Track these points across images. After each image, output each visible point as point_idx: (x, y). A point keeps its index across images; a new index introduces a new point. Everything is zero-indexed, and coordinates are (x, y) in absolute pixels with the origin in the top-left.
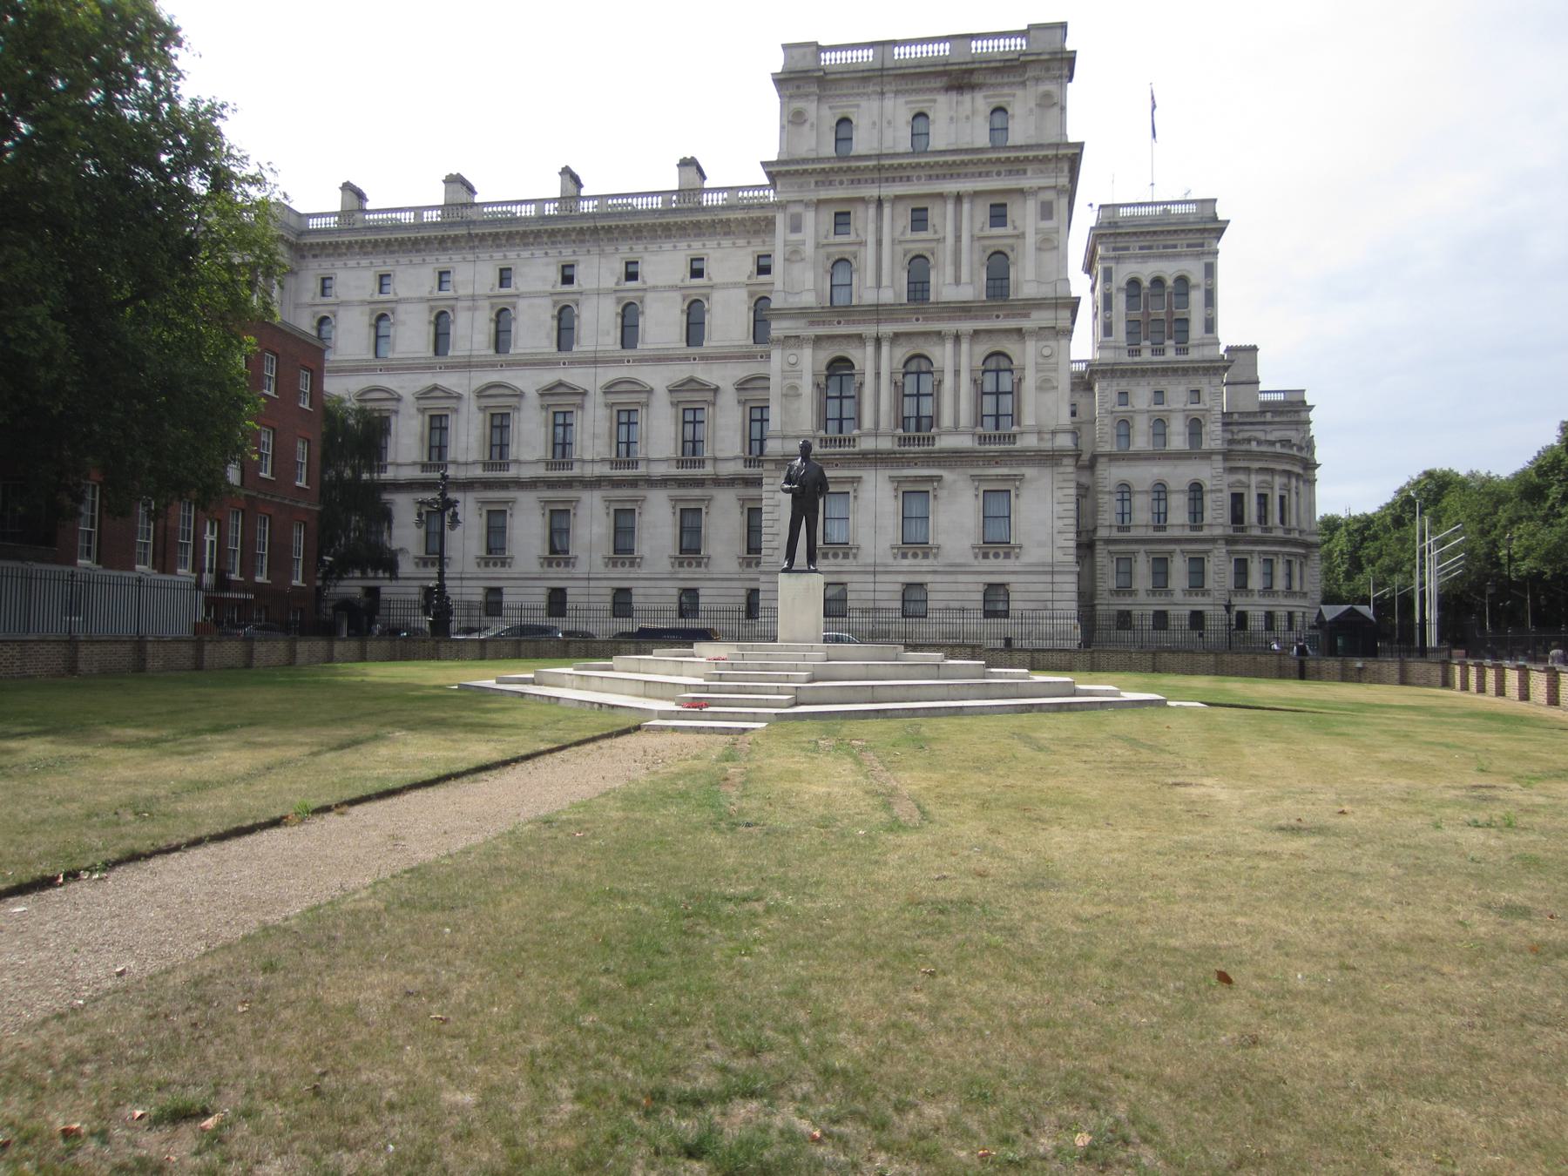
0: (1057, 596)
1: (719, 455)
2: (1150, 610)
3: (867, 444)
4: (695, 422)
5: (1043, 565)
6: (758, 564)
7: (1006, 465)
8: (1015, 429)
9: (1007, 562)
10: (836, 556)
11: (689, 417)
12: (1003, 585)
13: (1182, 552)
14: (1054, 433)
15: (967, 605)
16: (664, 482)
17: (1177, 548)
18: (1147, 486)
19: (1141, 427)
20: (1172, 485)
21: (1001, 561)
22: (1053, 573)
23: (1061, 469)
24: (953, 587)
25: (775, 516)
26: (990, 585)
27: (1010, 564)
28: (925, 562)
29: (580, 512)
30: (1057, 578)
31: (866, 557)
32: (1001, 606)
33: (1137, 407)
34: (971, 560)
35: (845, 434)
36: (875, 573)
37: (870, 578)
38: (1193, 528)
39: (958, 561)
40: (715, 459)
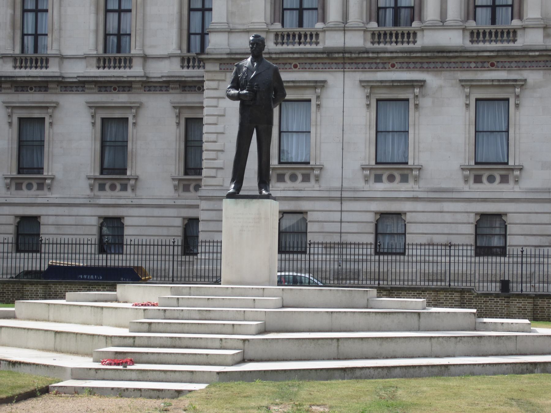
1: (150, 52)
6: (197, 187)
7: (503, 68)
8: (516, 23)
9: (504, 186)
10: (293, 178)
12: (499, 215)
15: (455, 240)
16: (81, 85)
24: (438, 217)
25: (219, 128)
28: (404, 186)
29: (141, 121)
31: (331, 178)
32: (496, 242)
34: (461, 185)
35: (306, 28)
37: (336, 205)
39: (444, 185)
40: (145, 58)
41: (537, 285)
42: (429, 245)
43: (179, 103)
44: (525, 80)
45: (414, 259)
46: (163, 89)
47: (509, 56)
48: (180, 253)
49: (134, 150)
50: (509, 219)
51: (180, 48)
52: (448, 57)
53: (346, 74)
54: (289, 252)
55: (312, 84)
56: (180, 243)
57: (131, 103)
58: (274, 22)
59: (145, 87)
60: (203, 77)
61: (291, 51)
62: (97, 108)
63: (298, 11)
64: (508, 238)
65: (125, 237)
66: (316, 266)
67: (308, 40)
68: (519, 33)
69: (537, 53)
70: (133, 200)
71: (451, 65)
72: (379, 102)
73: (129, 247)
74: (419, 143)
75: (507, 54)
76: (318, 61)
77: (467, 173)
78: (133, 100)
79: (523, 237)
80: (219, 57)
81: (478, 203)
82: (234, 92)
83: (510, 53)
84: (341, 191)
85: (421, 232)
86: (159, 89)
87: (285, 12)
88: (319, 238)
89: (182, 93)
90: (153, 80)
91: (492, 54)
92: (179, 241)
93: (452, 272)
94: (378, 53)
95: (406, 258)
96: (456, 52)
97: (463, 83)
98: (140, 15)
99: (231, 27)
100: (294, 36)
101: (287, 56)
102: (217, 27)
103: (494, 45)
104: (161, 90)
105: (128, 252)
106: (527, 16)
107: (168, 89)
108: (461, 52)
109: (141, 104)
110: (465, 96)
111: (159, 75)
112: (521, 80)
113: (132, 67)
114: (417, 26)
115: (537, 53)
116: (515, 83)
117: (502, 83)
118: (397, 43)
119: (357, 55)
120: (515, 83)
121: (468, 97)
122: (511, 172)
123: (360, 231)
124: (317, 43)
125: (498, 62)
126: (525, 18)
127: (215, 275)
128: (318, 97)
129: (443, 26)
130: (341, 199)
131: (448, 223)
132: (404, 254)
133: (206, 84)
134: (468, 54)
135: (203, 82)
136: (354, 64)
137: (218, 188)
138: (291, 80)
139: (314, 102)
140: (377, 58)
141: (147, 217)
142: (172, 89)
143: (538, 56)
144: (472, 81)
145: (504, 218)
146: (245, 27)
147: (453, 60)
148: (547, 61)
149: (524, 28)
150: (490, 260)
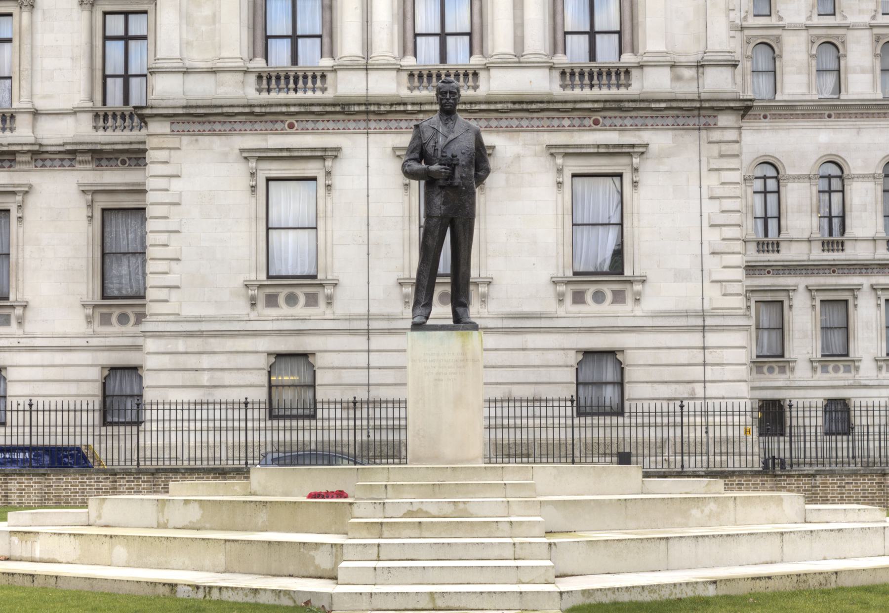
0: (711, 373)
2: (819, 397)
3: (349, 85)
4: (126, 38)
5: (686, 314)
6: (141, 317)
7: (613, 128)
8: (628, 58)
9: (619, 308)
10: (292, 300)
11: (116, 26)
12: (612, 353)
13: (874, 288)
14: (700, 66)
15: (546, 392)
17: (865, 281)
18: (808, 166)
19: (796, 51)
20: (854, 166)
21: (607, 307)
22: (704, 329)
23: (716, 135)
24: (519, 358)
25: (171, 225)
26: (588, 353)
27: (625, 313)
29: (30, 213)
30: (712, 339)
31: (349, 301)
32: (610, 394)
33: (787, 20)
34: (551, 306)
36: (368, 332)
37: (359, 342)
38: (828, 245)
39: (527, 309)
41: (672, 458)
42: (508, 401)
43: (91, 185)
44: (646, 146)
45: (211, 424)
46: (64, 163)
47: (620, 109)
48: (97, 422)
49: (20, 261)
50: (629, 358)
51: (92, 100)
52: (527, 110)
53: (371, 137)
54: (284, 417)
55: (319, 154)
56: (97, 407)
57: (14, 186)
58: (254, 56)
59: (36, 160)
60: (144, 143)
61: (283, 102)
62: (95, 192)
63: (289, 40)
64: (627, 387)
65: (9, 400)
66: (717, 434)
67: (310, 84)
68: (634, 73)
69: (663, 105)
70: (20, 340)
71: (532, 123)
72: (270, 183)
73: (15, 414)
74: (486, 242)
75: (617, 106)
76: (326, 117)
77: (562, 288)
78: (17, 182)
79: (649, 385)
80: (171, 111)
81: (580, 335)
82: (415, 166)
83: (622, 105)
84: (368, 319)
85: (493, 381)
86: (57, 163)
87: (269, 40)
88: (336, 394)
89: (96, 170)
90: (49, 149)
91: (596, 105)
92: (97, 403)
93: (685, 439)
94: (421, 104)
95: (320, 423)
96: (542, 102)
97: (553, 151)
98: (26, 48)
99: (187, 66)
100: (287, 78)
101: (279, 109)
102: (166, 65)
103: (587, 93)
104: (62, 166)
105: (15, 423)
106: (645, 47)
107: (73, 163)
108: (549, 102)
109: (30, 186)
110: (555, 170)
111: (61, 142)
112: (640, 146)
113: (15, 129)
114: (478, 63)
115: (663, 105)
116: (631, 150)
117: (611, 150)
118: (296, 90)
119: (388, 108)
120: (631, 150)
121: (560, 171)
122: (628, 286)
123: (398, 382)
124: (324, 90)
125: (605, 118)
126: (641, 51)
127: (173, 455)
128: (328, 173)
129: (519, 62)
130: (368, 332)
131: (534, 366)
132: (313, 417)
133: (151, 155)
134: (559, 106)
135: (144, 151)
136: (383, 122)
137: (172, 318)
138: (286, 147)
139: (321, 181)
140: (420, 112)
141: (42, 366)
142: (80, 162)
143: (666, 109)
144: (567, 146)
145: (619, 357)
146: (209, 65)
147: (535, 115)
148: (678, 117)
149: (641, 66)
150: (602, 422)
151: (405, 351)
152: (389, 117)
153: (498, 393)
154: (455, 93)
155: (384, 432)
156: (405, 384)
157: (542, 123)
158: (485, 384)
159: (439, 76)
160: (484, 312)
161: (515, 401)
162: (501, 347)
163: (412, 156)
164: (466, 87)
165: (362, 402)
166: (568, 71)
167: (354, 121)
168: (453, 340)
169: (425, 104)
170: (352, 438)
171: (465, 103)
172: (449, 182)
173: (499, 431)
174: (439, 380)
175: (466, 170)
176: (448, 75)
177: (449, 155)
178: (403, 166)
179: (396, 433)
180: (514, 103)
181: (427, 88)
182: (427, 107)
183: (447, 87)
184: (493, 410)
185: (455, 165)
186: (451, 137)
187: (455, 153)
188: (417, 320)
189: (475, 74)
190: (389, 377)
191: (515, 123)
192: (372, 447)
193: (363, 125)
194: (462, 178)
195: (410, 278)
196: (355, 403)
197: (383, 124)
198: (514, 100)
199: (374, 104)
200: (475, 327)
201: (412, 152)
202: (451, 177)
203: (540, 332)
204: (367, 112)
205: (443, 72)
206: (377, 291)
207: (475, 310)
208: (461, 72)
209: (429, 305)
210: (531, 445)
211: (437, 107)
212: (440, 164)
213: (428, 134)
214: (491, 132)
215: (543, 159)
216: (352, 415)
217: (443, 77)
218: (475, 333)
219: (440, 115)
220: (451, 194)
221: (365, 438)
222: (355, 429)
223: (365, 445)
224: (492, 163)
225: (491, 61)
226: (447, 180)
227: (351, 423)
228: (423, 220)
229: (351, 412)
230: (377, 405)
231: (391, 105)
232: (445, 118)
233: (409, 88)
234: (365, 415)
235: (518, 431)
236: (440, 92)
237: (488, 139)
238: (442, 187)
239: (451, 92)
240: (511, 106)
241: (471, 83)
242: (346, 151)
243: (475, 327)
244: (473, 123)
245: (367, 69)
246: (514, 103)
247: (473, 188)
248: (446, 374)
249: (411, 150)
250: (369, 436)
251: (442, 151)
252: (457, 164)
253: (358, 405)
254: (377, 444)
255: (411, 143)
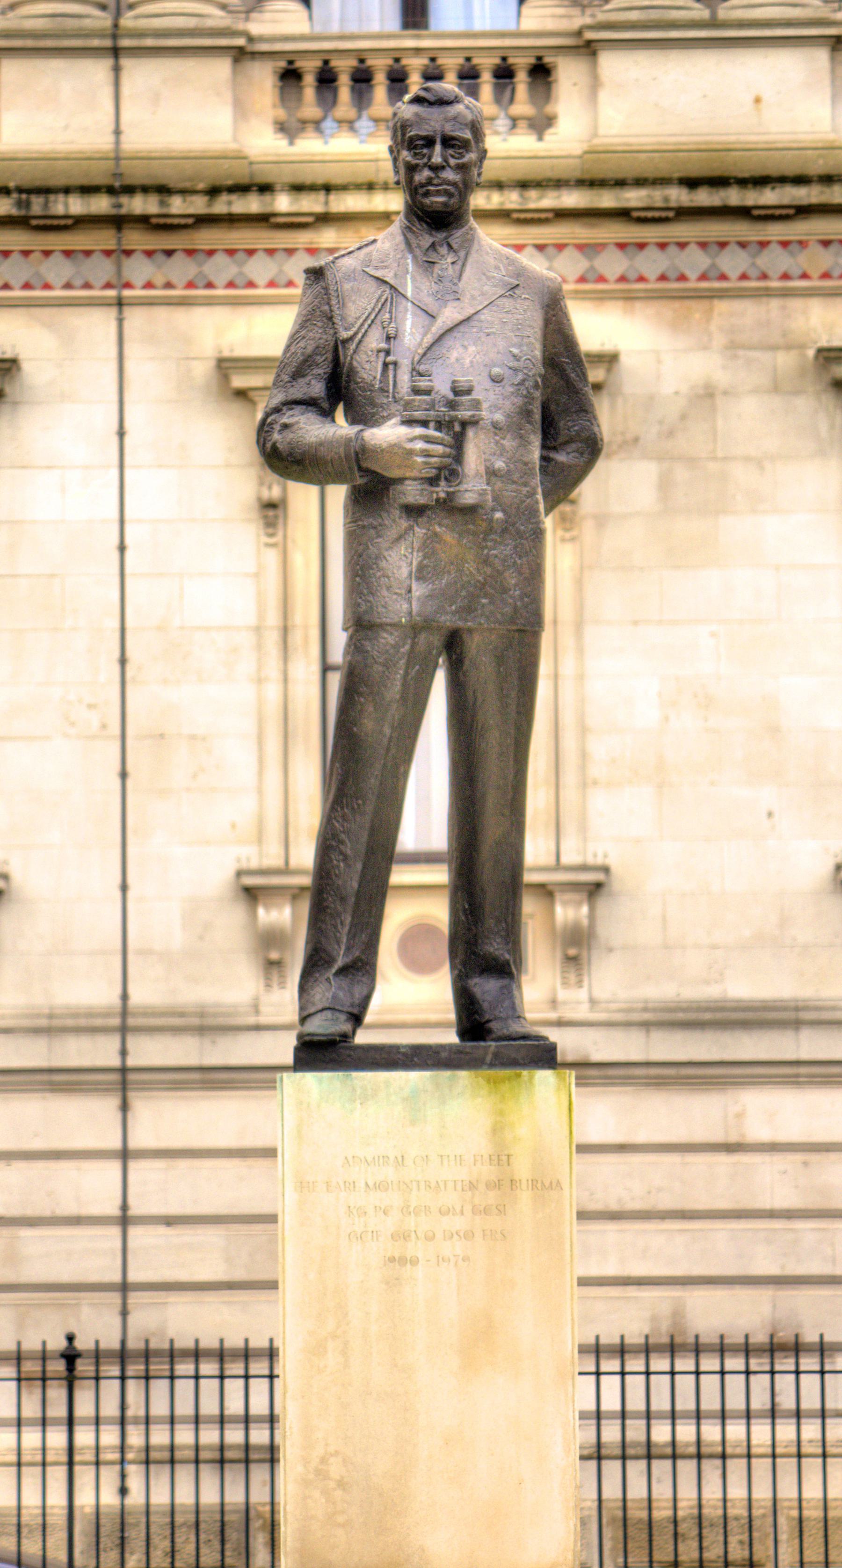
24: (711, 1182)
37: (89, 1120)
39: (742, 987)
52: (744, 213)
53: (135, 318)
71: (764, 260)
74: (583, 730)
94: (328, 188)
96: (800, 180)
114: (550, 25)
119: (198, 205)
123: (239, 1274)
129: (713, 23)
131: (772, 1214)
140: (325, 219)
147: (775, 231)
151: (270, 1153)
152: (206, 238)
153: (630, 1318)
154: (465, 145)
155: (185, 1474)
156: (272, 1285)
157: (802, 261)
158: (583, 1282)
159: (397, 80)
160: (575, 1001)
161: (698, 1349)
162: (641, 1137)
163: (298, 391)
164: (502, 123)
165: (98, 1355)
166: (310, 67)
167: (68, 253)
168: (458, 1108)
169: (344, 188)
170: (57, 1498)
171: (499, 185)
172: (441, 490)
173: (637, 1469)
174: (402, 1261)
175: (509, 443)
176: (433, 75)
177: (442, 387)
178: (264, 429)
179: (234, 1474)
180: (691, 183)
181: (350, 125)
182: (352, 202)
183: (435, 121)
184: (611, 1385)
185: (464, 424)
186: (449, 314)
187: (463, 380)
188: (319, 1026)
189: (541, 72)
190: (205, 1256)
191: (694, 261)
192: (136, 1536)
193: (101, 269)
194: (491, 473)
195: (286, 870)
196: (70, 1357)
197: (180, 269)
198: (695, 171)
199: (145, 189)
200: (544, 1056)
201: (297, 374)
202: (449, 470)
203: (794, 1081)
204: (118, 222)
205: (415, 65)
206: (159, 921)
207: (539, 992)
208: (486, 63)
209: (362, 968)
210: (764, 1526)
211: (394, 202)
212: (409, 422)
213: (357, 305)
214: (601, 297)
215: (804, 404)
216: (58, 1410)
217: (415, 84)
218: (544, 1077)
219: (407, 230)
220: (449, 537)
221: (109, 1498)
222: (71, 1464)
223: (109, 1528)
224: (608, 417)
225: (601, 17)
226: (433, 481)
227: (57, 1438)
228: (339, 639)
229: (57, 1394)
230: (159, 1367)
231: (213, 192)
232: (427, 240)
233: (282, 127)
234: (110, 1408)
235: (711, 1469)
236: (410, 142)
237: (594, 327)
238: (414, 511)
239: (448, 142)
240: (679, 196)
241: (522, 106)
242: (36, 372)
243: (544, 1056)
244: (535, 264)
245: (116, 52)
246: (691, 183)
247: (533, 512)
248: (430, 1237)
249: (294, 368)
250: (123, 1491)
251: (416, 372)
252: (474, 422)
253: (83, 1367)
254: (159, 1521)
255: (294, 338)
